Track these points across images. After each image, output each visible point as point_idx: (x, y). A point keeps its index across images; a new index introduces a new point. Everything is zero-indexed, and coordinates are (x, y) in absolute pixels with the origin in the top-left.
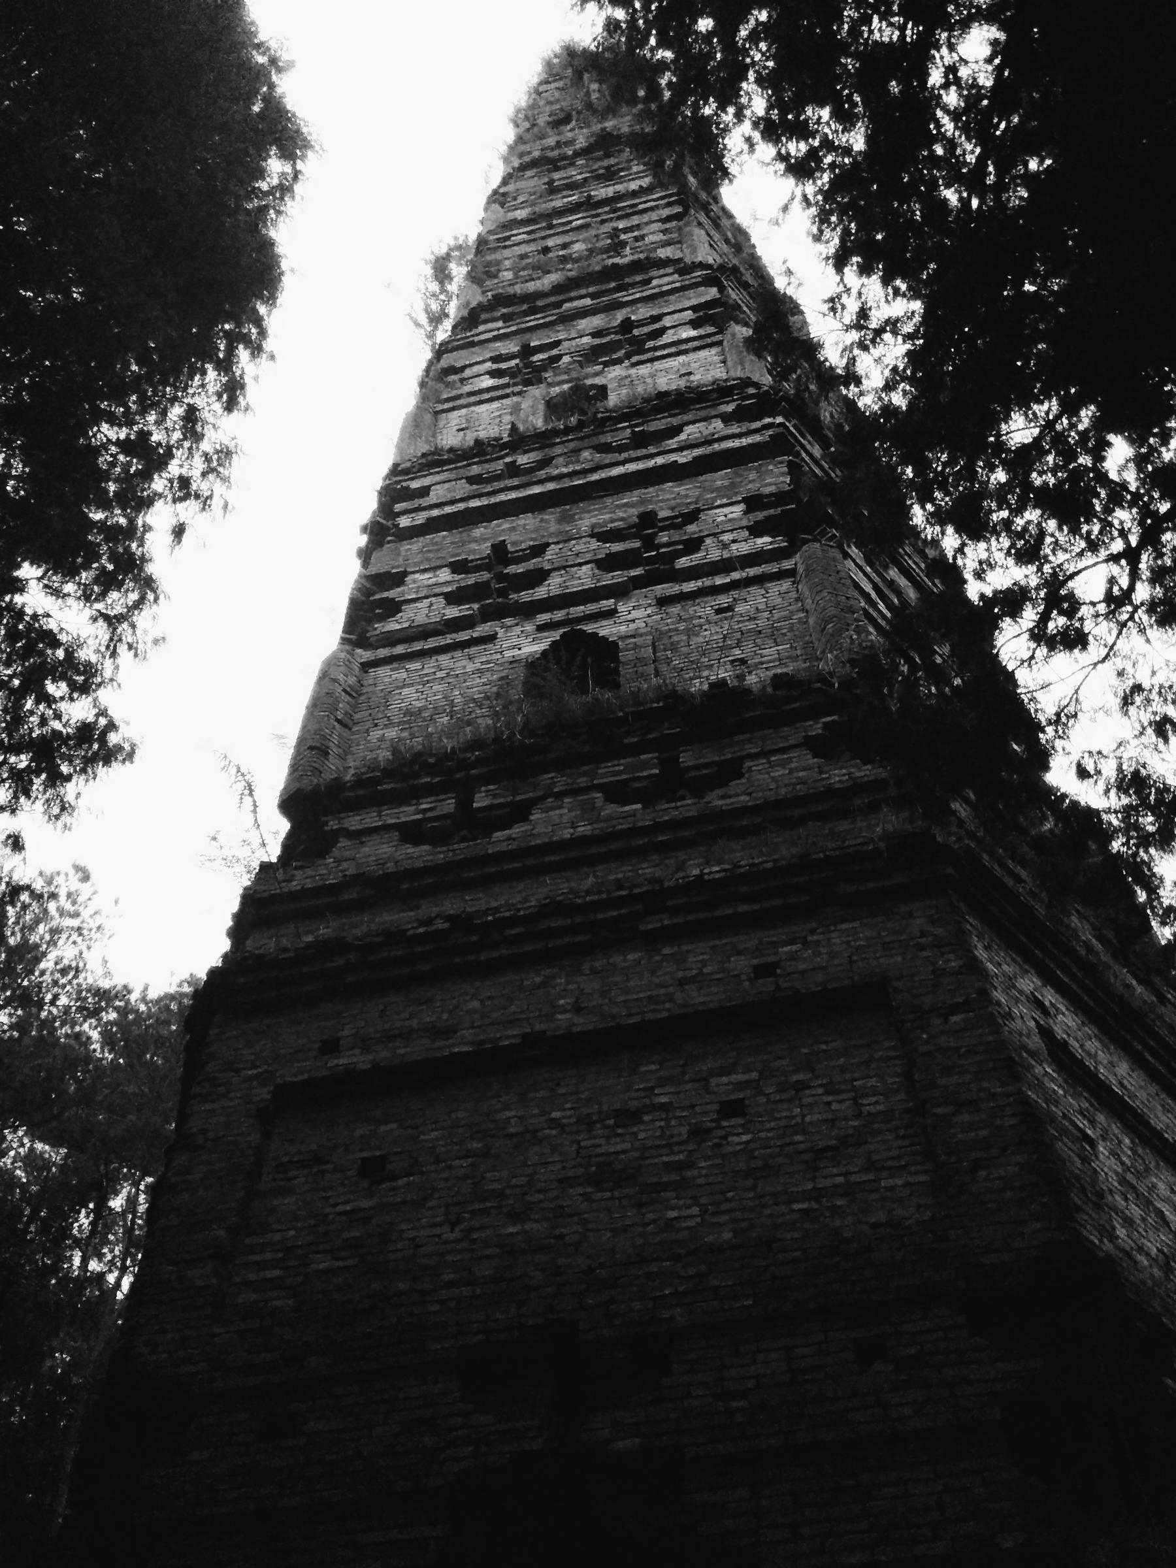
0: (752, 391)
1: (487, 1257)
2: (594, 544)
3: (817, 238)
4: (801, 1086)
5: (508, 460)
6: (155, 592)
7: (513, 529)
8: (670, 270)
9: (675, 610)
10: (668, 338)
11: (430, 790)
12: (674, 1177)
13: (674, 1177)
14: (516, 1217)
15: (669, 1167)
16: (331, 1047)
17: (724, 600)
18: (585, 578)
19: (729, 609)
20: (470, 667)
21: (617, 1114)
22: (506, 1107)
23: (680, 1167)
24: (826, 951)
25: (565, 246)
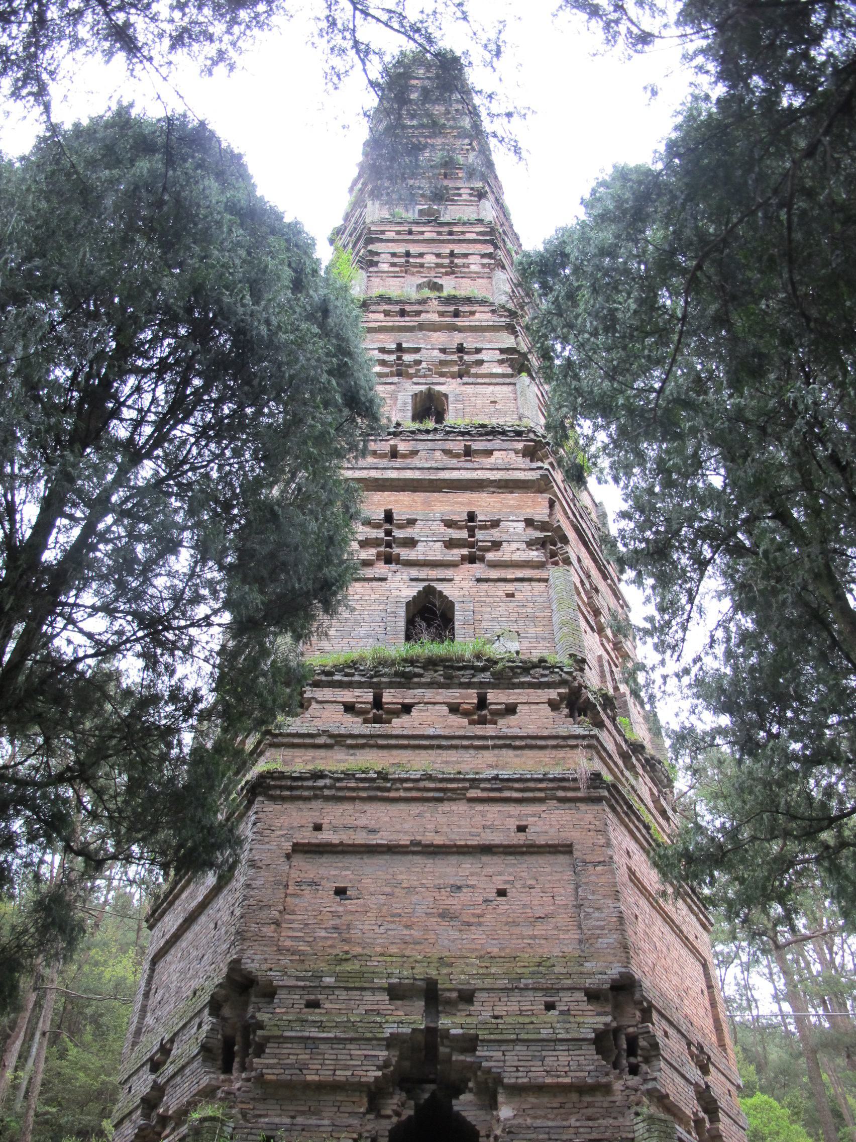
0: (532, 436)
1: (415, 41)
2: (442, 528)
3: (626, 501)
4: (531, 887)
5: (392, 442)
6: (70, 943)
7: (396, 501)
8: (487, 309)
9: (484, 586)
10: (484, 369)
11: (360, 685)
12: (476, 920)
13: (476, 920)
14: (407, 927)
15: (474, 915)
16: (318, 828)
17: (510, 587)
18: (436, 552)
19: (512, 595)
20: (374, 597)
21: (452, 886)
22: (401, 873)
23: (479, 916)
24: (549, 822)
25: (421, 255)
